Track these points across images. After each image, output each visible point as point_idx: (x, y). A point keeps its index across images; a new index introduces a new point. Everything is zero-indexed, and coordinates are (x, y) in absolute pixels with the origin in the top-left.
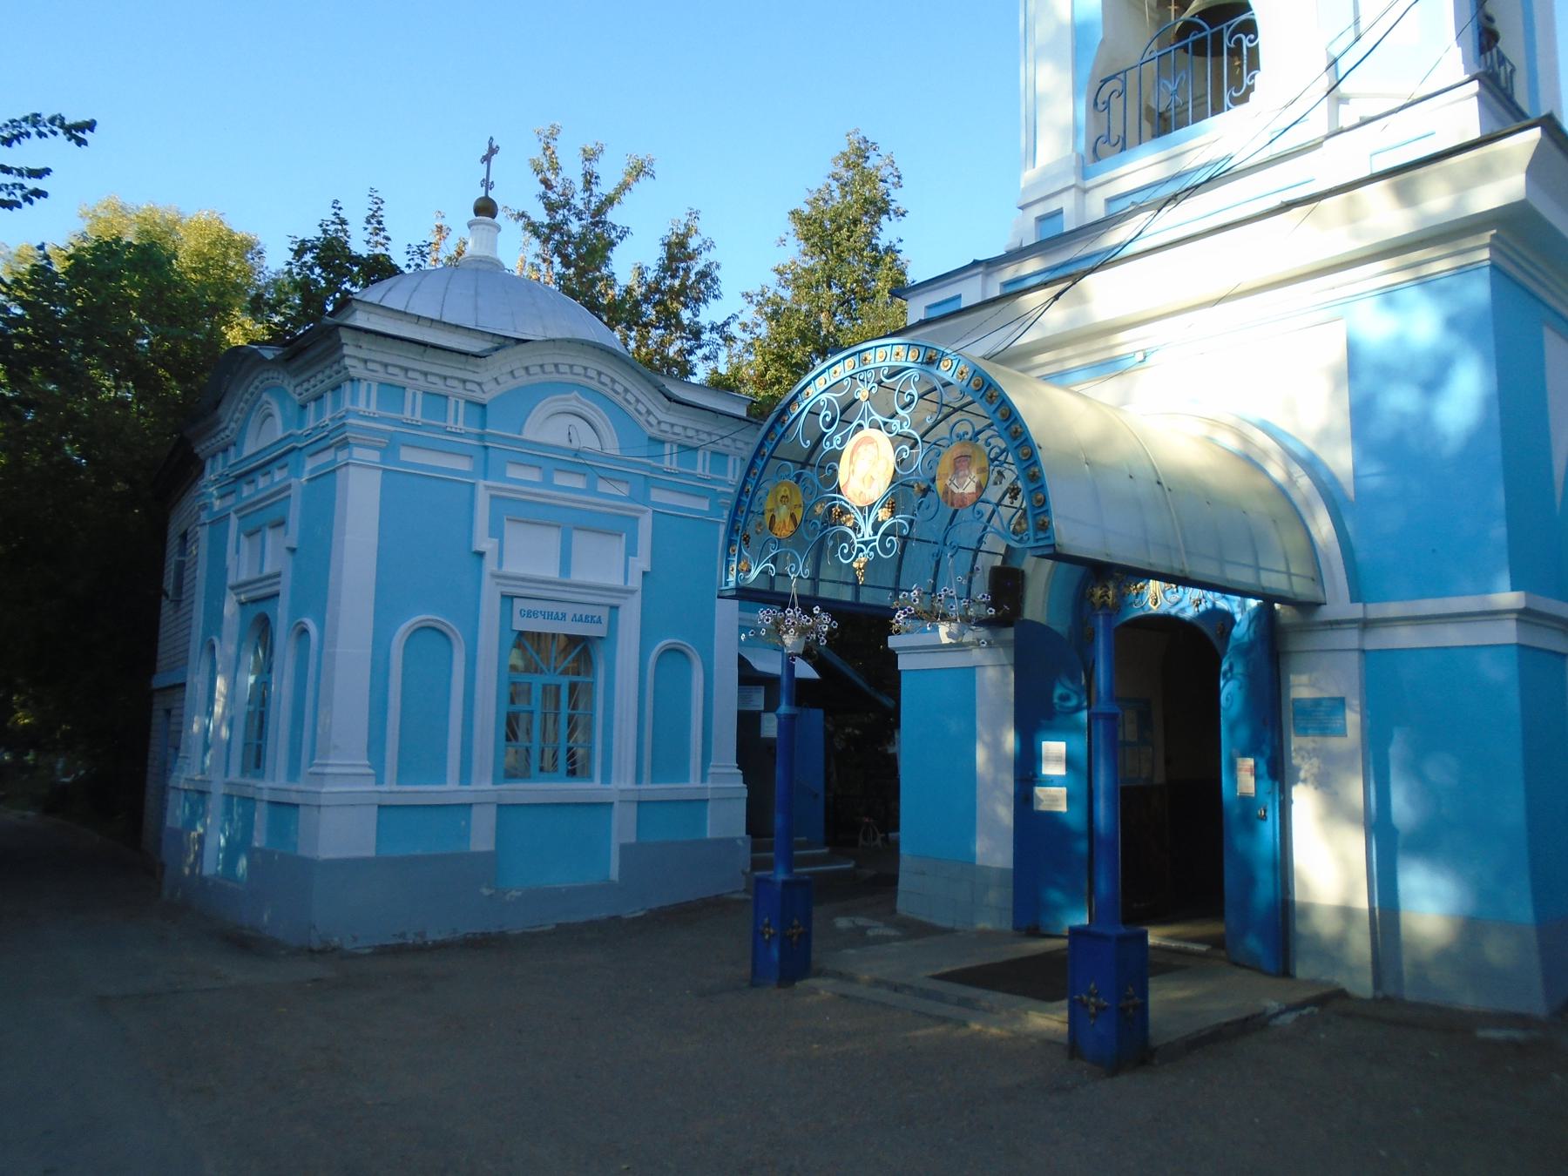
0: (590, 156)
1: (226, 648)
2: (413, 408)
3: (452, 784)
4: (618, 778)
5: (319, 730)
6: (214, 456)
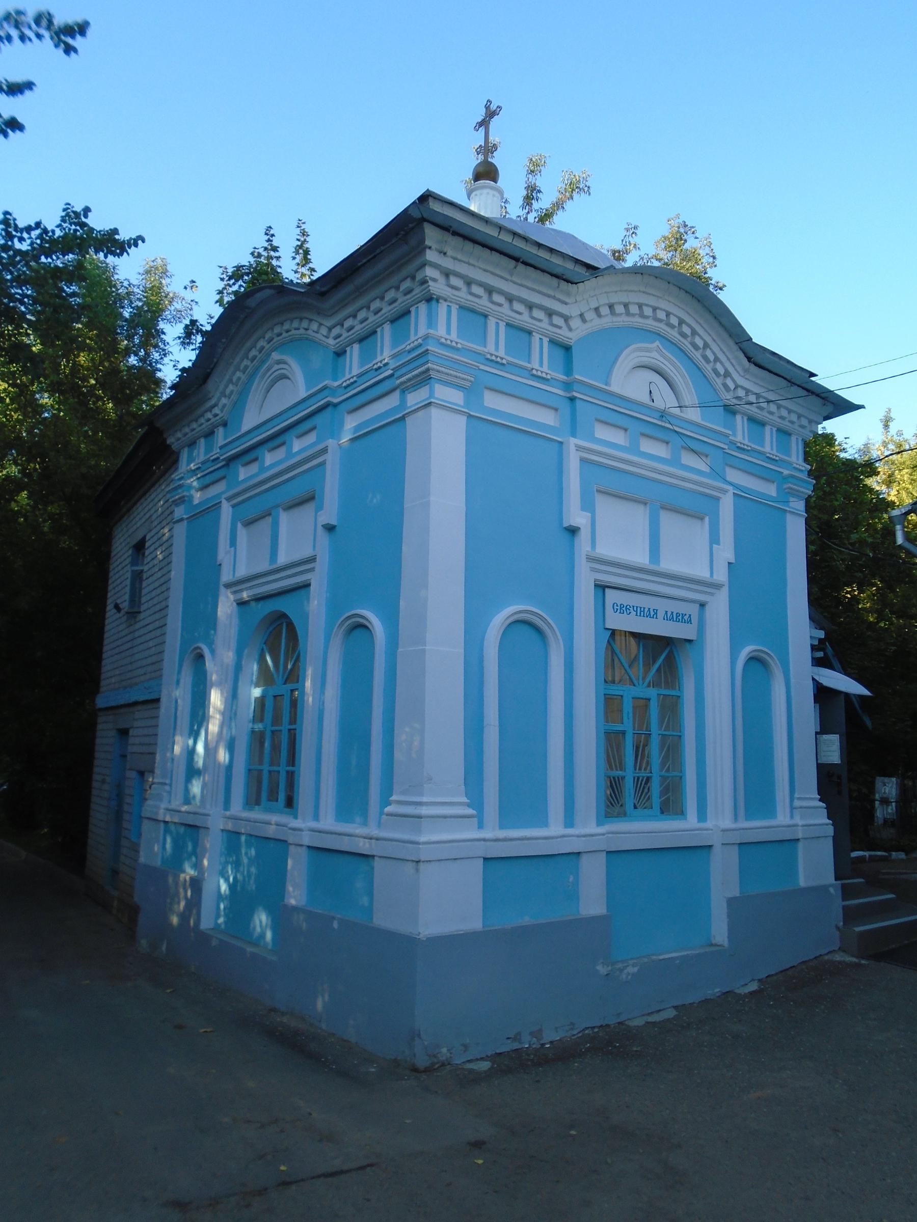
0: (534, 168)
1: (221, 658)
2: (496, 343)
3: (556, 828)
4: (713, 814)
5: (398, 755)
6: (192, 444)
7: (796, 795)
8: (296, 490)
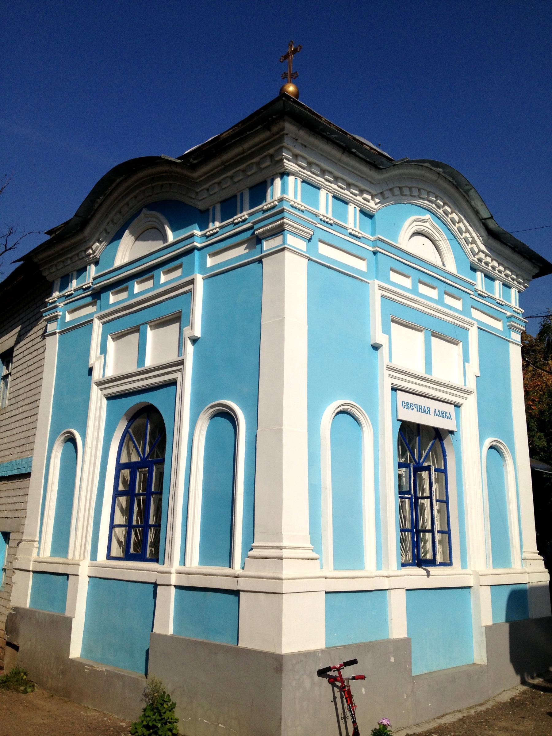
7: (524, 550)
8: (166, 310)
